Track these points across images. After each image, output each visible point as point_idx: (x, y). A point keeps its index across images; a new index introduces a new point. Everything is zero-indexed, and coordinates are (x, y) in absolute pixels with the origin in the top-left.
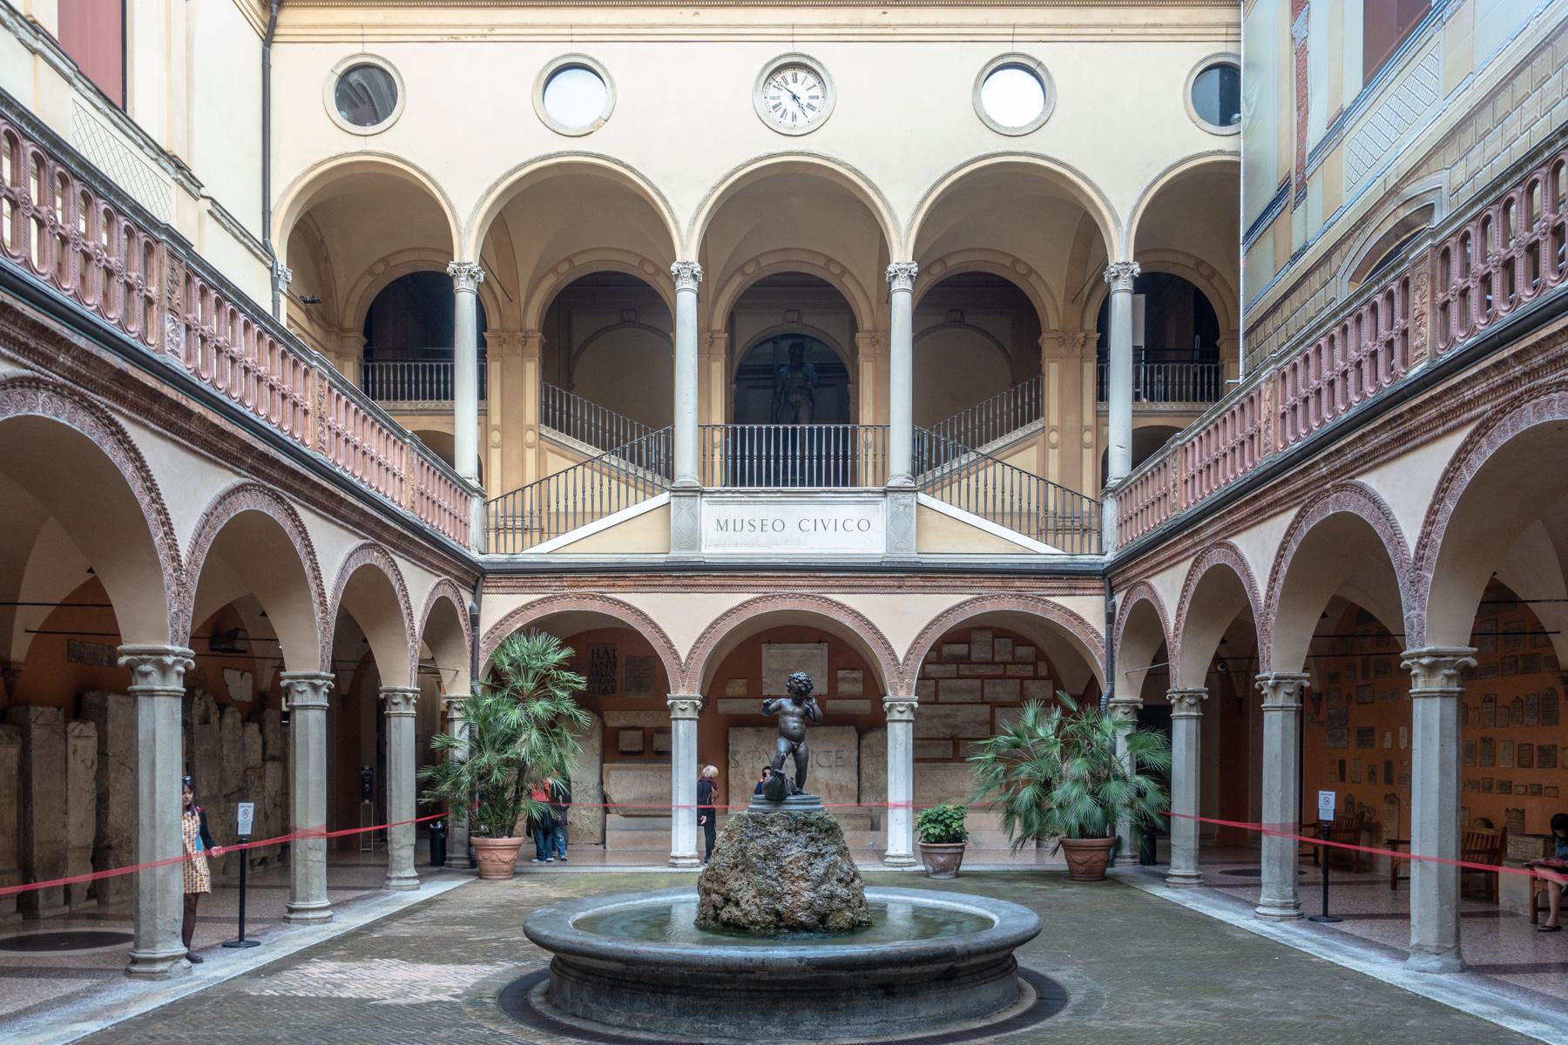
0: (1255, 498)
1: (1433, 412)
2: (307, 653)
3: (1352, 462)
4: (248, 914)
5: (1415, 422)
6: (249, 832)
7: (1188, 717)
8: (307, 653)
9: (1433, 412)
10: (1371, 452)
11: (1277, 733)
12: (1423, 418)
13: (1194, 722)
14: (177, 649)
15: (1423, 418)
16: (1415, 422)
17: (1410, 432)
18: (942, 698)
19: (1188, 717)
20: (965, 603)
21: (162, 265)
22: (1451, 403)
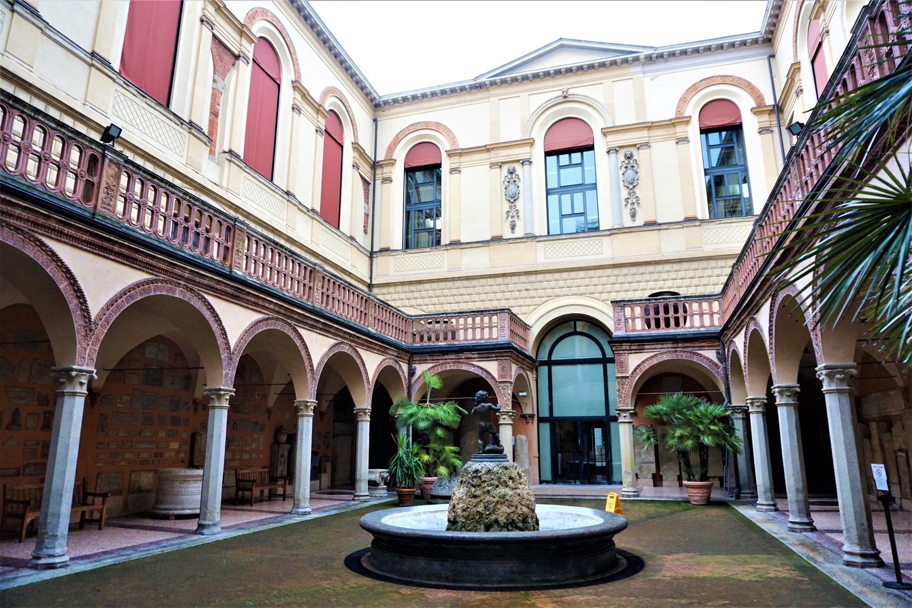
0: (71, 226)
1: (253, 300)
2: (364, 401)
3: (206, 285)
4: (895, 528)
5: (244, 296)
6: (596, 429)
7: (757, 412)
8: (364, 401)
9: (253, 300)
10: (217, 289)
11: (836, 412)
12: (250, 298)
13: (792, 408)
14: (226, 388)
15: (250, 298)
16: (244, 296)
17: (136, 260)
18: (553, 198)
19: (757, 412)
20: (876, 162)
21: (287, 446)
22: (260, 302)
